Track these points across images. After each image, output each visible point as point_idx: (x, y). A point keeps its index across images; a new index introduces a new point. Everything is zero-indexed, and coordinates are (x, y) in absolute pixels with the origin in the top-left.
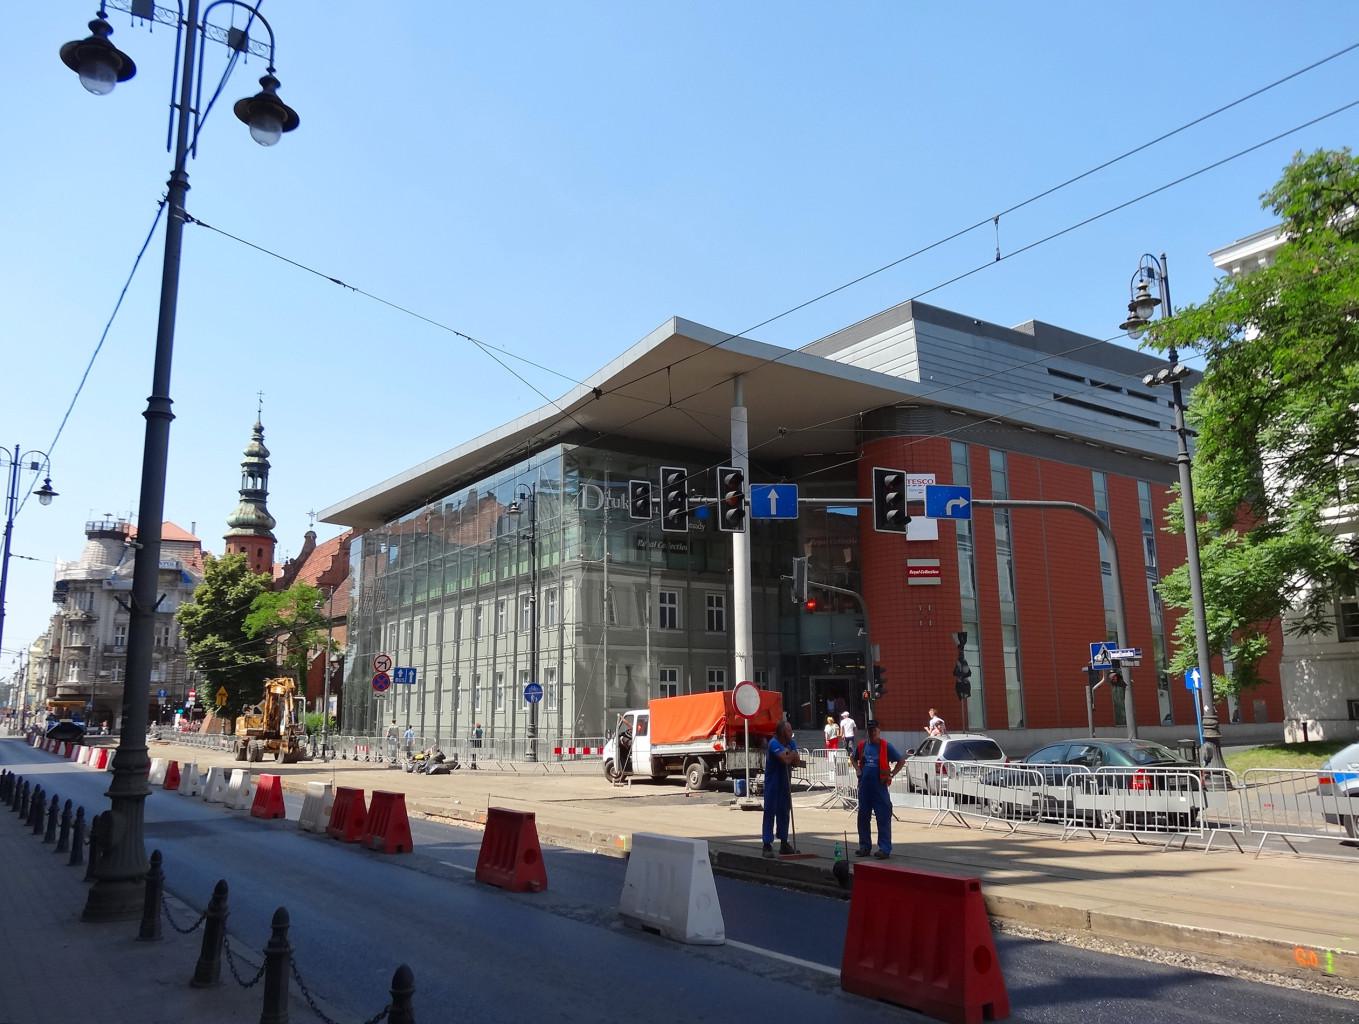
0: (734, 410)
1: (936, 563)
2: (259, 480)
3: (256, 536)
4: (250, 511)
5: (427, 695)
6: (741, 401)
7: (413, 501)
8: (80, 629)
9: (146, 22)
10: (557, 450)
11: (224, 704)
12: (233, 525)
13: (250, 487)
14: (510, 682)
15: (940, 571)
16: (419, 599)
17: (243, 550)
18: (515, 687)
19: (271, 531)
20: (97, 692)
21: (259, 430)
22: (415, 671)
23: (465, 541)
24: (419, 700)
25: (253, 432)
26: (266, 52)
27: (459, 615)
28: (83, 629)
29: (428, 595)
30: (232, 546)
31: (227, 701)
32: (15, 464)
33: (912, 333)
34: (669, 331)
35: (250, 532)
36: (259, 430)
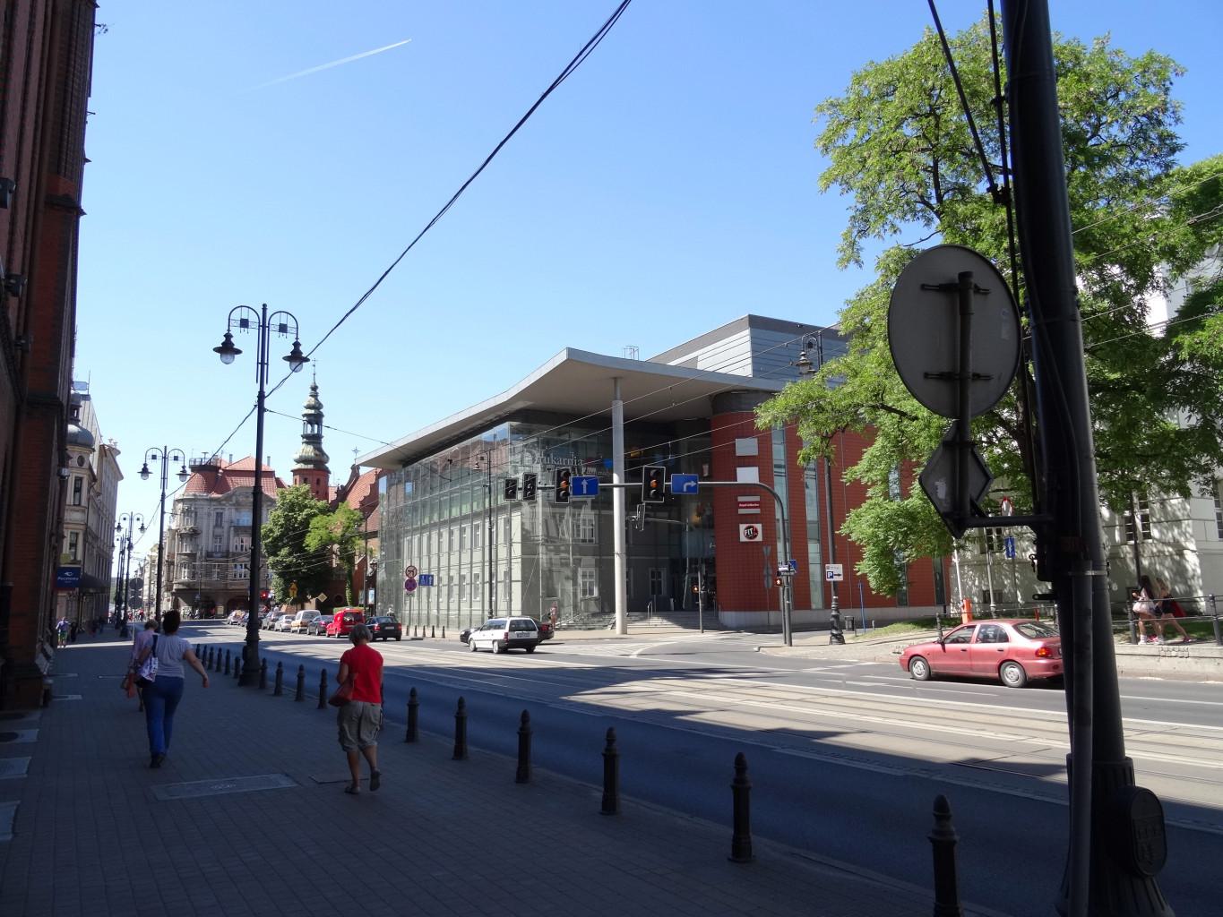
0: (614, 402)
1: (757, 498)
2: (316, 426)
3: (314, 469)
4: (309, 451)
5: (513, 584)
6: (619, 395)
7: (420, 452)
8: (189, 540)
9: (246, 329)
10: (506, 426)
11: (295, 596)
12: (298, 461)
13: (309, 432)
14: (469, 582)
15: (760, 504)
16: (414, 527)
17: (305, 481)
18: (471, 584)
19: (327, 465)
20: (203, 587)
21: (314, 388)
22: (432, 576)
23: (912, 185)
24: (505, 588)
25: (310, 390)
26: (294, 331)
27: (429, 538)
28: (191, 540)
29: (461, 510)
30: (298, 477)
31: (297, 594)
32: (165, 458)
33: (748, 338)
34: (563, 357)
35: (311, 466)
36: (314, 388)
